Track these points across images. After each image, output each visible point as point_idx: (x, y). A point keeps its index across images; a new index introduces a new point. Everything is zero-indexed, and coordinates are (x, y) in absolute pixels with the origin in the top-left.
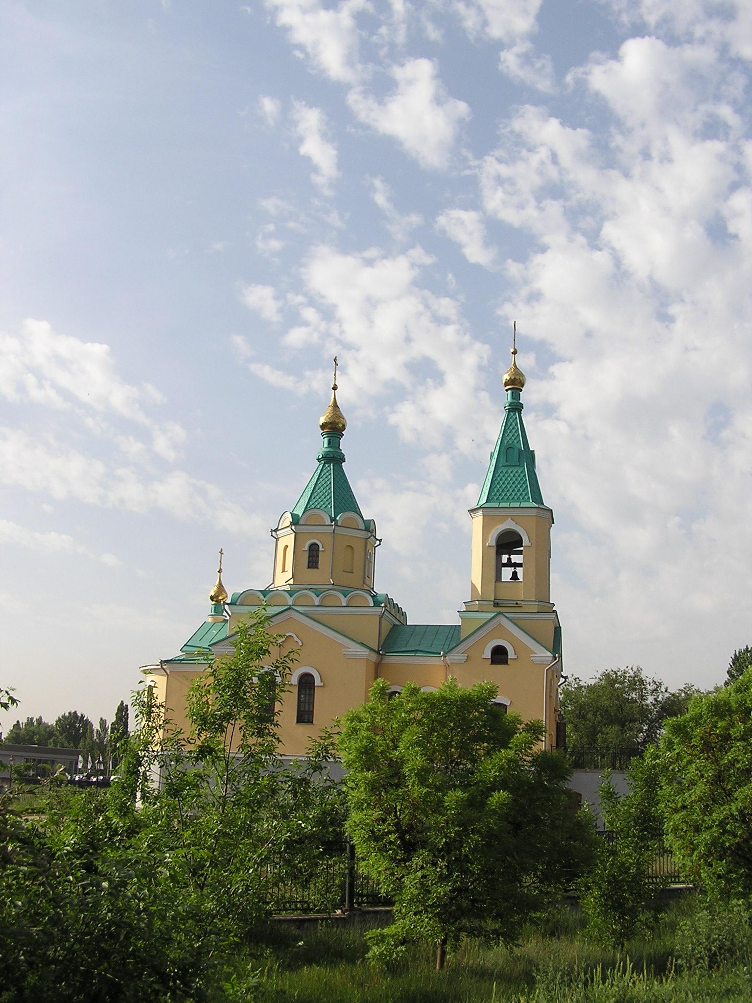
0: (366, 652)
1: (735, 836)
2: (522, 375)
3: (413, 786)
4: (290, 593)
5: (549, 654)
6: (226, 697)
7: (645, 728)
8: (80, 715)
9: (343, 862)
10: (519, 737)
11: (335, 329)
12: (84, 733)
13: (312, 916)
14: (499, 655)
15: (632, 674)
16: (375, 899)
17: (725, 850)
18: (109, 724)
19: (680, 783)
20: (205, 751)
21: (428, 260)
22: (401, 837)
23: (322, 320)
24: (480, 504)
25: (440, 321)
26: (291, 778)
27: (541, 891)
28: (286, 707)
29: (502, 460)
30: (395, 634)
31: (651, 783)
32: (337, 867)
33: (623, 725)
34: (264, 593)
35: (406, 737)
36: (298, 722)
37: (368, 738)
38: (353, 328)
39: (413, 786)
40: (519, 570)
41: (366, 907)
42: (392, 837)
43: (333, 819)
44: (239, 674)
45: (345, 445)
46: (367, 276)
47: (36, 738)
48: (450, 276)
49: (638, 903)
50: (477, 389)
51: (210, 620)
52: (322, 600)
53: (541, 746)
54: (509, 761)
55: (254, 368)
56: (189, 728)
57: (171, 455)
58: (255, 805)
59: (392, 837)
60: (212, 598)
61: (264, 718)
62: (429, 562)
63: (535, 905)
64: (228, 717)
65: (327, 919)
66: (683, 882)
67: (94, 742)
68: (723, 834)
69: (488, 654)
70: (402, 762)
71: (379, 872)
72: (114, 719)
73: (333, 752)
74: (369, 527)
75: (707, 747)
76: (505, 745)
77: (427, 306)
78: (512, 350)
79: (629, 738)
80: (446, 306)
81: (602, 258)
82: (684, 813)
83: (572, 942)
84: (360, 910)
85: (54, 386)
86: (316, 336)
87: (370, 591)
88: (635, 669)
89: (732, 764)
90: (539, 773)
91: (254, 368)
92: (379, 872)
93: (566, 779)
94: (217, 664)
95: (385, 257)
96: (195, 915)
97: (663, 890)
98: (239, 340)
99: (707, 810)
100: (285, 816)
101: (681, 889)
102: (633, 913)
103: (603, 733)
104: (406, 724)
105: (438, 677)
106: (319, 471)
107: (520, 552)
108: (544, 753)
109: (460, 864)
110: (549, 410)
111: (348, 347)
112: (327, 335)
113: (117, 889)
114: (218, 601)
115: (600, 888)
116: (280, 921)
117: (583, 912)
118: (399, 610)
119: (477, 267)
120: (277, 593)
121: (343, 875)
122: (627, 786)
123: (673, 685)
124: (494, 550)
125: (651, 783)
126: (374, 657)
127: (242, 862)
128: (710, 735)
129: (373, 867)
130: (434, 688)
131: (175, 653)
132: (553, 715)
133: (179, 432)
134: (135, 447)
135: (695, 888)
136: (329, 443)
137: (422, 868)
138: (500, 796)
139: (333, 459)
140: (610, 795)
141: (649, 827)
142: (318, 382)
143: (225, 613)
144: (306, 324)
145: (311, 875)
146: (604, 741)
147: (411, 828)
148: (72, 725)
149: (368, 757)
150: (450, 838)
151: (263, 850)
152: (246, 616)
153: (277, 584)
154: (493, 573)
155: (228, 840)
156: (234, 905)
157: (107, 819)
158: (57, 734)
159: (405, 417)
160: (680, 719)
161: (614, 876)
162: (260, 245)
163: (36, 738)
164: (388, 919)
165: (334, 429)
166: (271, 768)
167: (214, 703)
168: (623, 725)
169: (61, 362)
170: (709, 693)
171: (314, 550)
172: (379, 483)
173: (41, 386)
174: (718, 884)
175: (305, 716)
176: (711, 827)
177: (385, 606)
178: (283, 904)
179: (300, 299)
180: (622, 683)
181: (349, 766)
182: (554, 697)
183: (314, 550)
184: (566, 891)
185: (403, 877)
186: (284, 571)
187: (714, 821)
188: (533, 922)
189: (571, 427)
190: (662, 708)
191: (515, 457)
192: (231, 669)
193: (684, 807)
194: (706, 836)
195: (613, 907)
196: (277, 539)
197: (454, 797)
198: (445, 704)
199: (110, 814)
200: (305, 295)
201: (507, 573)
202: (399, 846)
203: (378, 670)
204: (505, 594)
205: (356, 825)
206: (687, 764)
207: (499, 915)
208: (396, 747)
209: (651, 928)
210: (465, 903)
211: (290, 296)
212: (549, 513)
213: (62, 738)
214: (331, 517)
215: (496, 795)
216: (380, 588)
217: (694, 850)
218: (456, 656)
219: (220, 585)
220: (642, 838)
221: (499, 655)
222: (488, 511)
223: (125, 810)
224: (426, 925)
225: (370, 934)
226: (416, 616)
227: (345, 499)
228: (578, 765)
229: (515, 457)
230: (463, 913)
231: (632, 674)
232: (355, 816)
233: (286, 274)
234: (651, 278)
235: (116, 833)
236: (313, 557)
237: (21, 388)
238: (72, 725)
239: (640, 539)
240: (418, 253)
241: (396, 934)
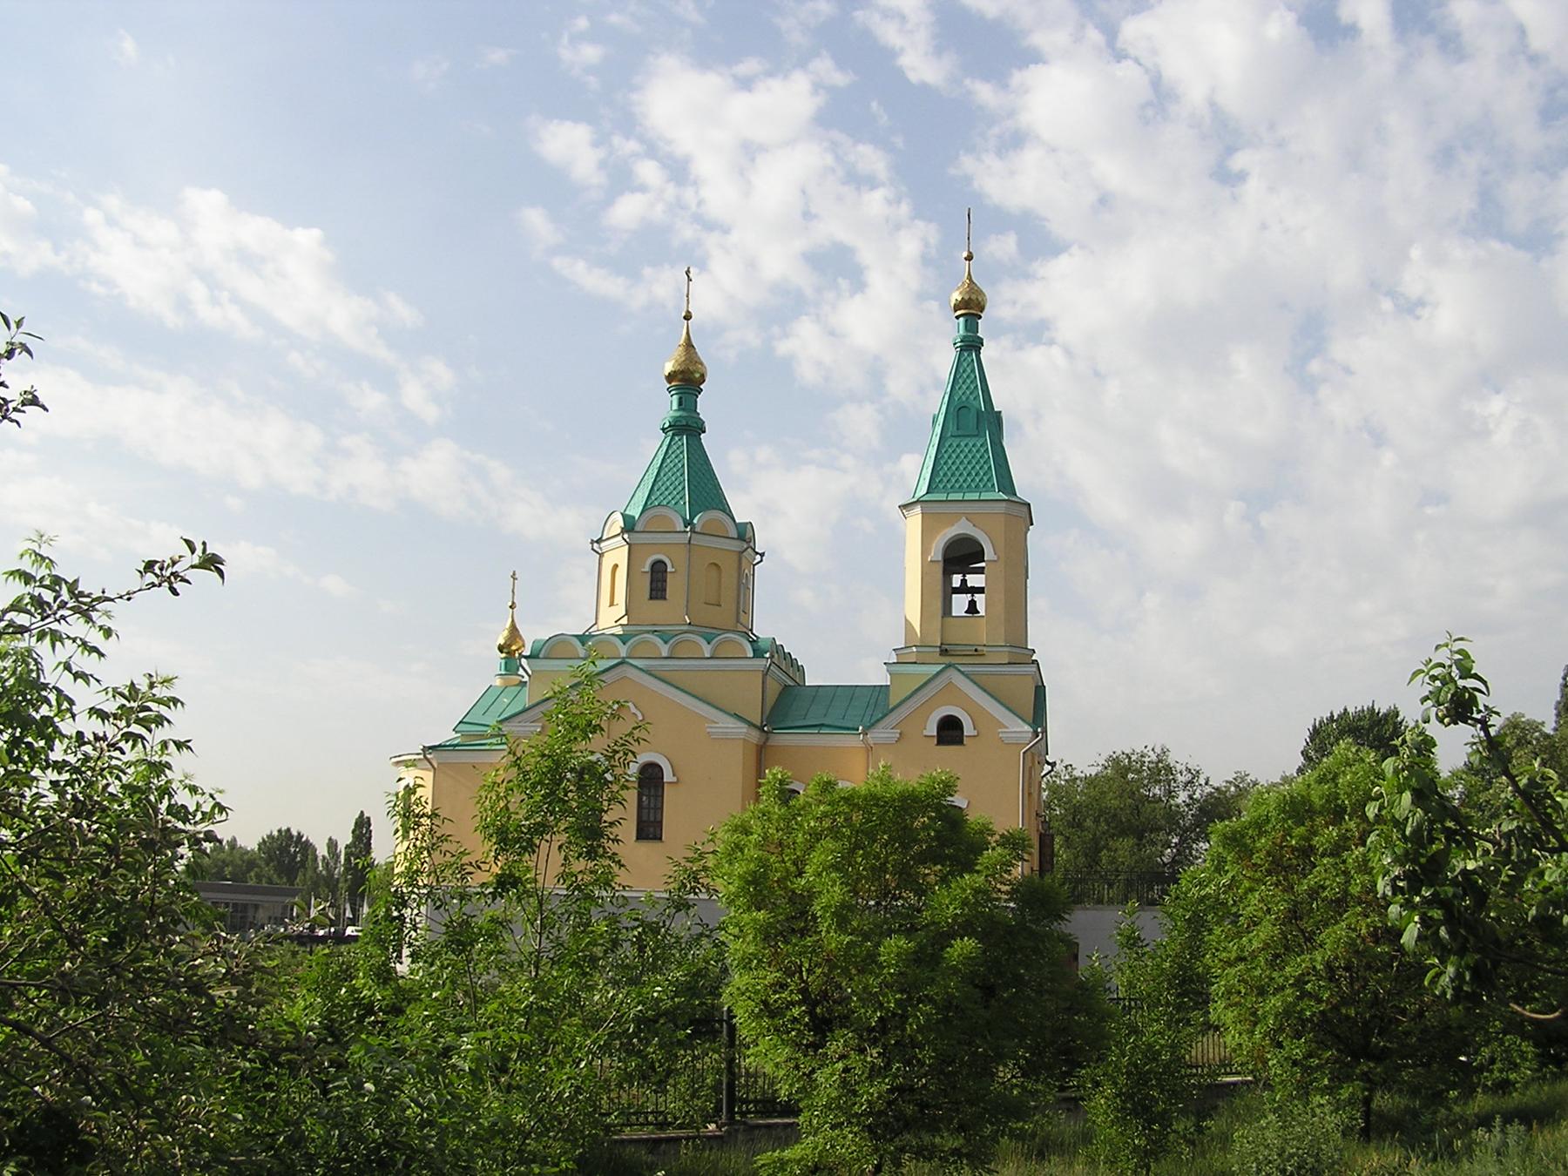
0: (743, 728)
1: (1320, 1001)
2: (980, 292)
3: (828, 932)
4: (623, 639)
5: (1027, 728)
6: (538, 798)
7: (1175, 840)
8: (295, 833)
9: (718, 1052)
10: (991, 855)
11: (689, 195)
12: (303, 862)
13: (671, 1133)
14: (950, 731)
15: (1154, 758)
16: (769, 1105)
17: (1303, 1022)
18: (341, 847)
19: (1234, 923)
20: (506, 882)
21: (840, 79)
22: (811, 1013)
23: (669, 180)
24: (918, 495)
25: (860, 181)
26: (643, 923)
27: (1024, 1088)
28: (622, 816)
29: (952, 428)
30: (788, 701)
31: (1197, 925)
32: (707, 1059)
33: (1140, 838)
34: (583, 639)
35: (817, 858)
36: (638, 838)
37: (759, 859)
38: (717, 190)
39: (828, 932)
40: (979, 598)
41: (752, 1119)
42: (796, 1011)
43: (703, 985)
44: (557, 763)
45: (705, 405)
46: (741, 106)
47: (227, 870)
48: (874, 105)
49: (1177, 1102)
50: (921, 297)
51: (498, 682)
52: (672, 649)
53: (1018, 871)
54: (977, 891)
55: (558, 263)
56: (481, 848)
57: (431, 413)
58: (586, 965)
59: (796, 1011)
60: (501, 649)
61: (591, 835)
62: (840, 587)
63: (1018, 1111)
64: (542, 829)
65: (694, 1138)
66: (1238, 1073)
67: (319, 875)
68: (1299, 998)
69: (932, 730)
70: (810, 895)
71: (777, 1065)
72: (349, 839)
73: (705, 881)
74: (745, 534)
75: (1277, 865)
76: (969, 867)
77: (838, 159)
78: (965, 254)
79: (1149, 857)
80: (871, 159)
81: (1126, 70)
82: (1241, 966)
83: (1071, 1165)
84: (745, 1123)
85: (235, 299)
86: (660, 207)
87: (747, 633)
88: (1158, 750)
89: (1314, 893)
90: (1021, 909)
91: (558, 263)
92: (777, 1065)
93: (1063, 919)
94: (522, 747)
95: (770, 74)
96: (503, 1129)
97: (1209, 1086)
98: (535, 219)
99: (1276, 962)
100: (634, 981)
101: (1235, 1084)
102: (1165, 1119)
103: (1109, 850)
104: (816, 836)
105: (858, 765)
106: (664, 448)
107: (981, 571)
108: (1026, 882)
109: (903, 1050)
110: (1037, 332)
111: (710, 226)
112: (680, 205)
113: (387, 1092)
114: (510, 654)
115: (1115, 1083)
116: (623, 1141)
117: (1086, 1121)
118: (793, 662)
119: (924, 87)
120: (603, 639)
121: (719, 1071)
122: (1158, 928)
123: (1218, 774)
124: (939, 568)
125: (1197, 925)
126: (755, 736)
127: (568, 1051)
128: (1282, 848)
129: (767, 1058)
130: (856, 777)
131: (446, 735)
132: (1034, 822)
133: (441, 372)
134: (372, 400)
135: (1256, 1081)
136: (680, 404)
137: (842, 1057)
138: (963, 947)
139: (687, 428)
140: (1132, 942)
141: (1190, 989)
142: (663, 285)
143: (521, 672)
144: (643, 189)
145: (669, 1073)
146: (1113, 861)
147: (825, 995)
148: (284, 850)
149: (757, 889)
150: (888, 1010)
151: (602, 1034)
152: (562, 673)
153: (602, 625)
154: (938, 604)
155: (543, 1019)
156: (556, 1117)
157: (353, 990)
158: (262, 864)
159: (805, 343)
160: (1234, 823)
161: (1136, 1066)
162: (566, 54)
163: (227, 870)
164: (790, 1135)
165: (687, 381)
166: (610, 908)
167: (520, 809)
168: (1140, 838)
169: (248, 259)
170: (1274, 785)
171: (658, 570)
172: (764, 454)
173: (215, 302)
174: (1293, 1075)
175: (649, 829)
176: (1283, 988)
177: (772, 657)
178: (632, 1115)
179: (632, 146)
180: (1139, 772)
181: (731, 902)
182: (1035, 795)
183: (658, 570)
184: (1062, 1089)
185: (813, 1071)
186: (612, 604)
187: (1287, 979)
188: (1013, 1135)
189: (1068, 352)
190: (1200, 809)
191: (972, 422)
192: (543, 755)
193: (1241, 959)
194: (1275, 1002)
195: (1135, 1113)
196: (601, 555)
197: (893, 947)
198: (877, 805)
199: (358, 983)
200: (641, 139)
201: (960, 603)
202: (806, 1025)
203: (762, 756)
204: (957, 636)
205: (739, 995)
206: (1246, 893)
207: (962, 1128)
208: (800, 874)
209: (1191, 1143)
210: (910, 1109)
211: (617, 140)
212: (1025, 509)
213: (269, 871)
214: (684, 519)
215: (957, 943)
216: (763, 628)
217: (1255, 1024)
218: (881, 734)
219: (514, 630)
220: (1179, 1007)
221: (950, 731)
222: (931, 506)
223: (385, 975)
224: (850, 1143)
225: (762, 1159)
226: (822, 669)
227: (705, 489)
228: (1078, 899)
229: (972, 422)
230: (907, 1125)
231: (1154, 758)
232: (738, 980)
233: (610, 106)
234: (1213, 104)
235: (370, 1010)
236: (658, 582)
237: (183, 304)
238: (284, 850)
239: (1179, 541)
240: (824, 66)
241: (802, 1159)
